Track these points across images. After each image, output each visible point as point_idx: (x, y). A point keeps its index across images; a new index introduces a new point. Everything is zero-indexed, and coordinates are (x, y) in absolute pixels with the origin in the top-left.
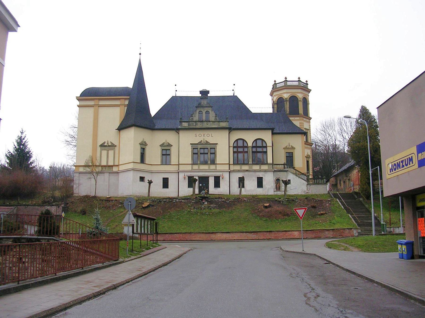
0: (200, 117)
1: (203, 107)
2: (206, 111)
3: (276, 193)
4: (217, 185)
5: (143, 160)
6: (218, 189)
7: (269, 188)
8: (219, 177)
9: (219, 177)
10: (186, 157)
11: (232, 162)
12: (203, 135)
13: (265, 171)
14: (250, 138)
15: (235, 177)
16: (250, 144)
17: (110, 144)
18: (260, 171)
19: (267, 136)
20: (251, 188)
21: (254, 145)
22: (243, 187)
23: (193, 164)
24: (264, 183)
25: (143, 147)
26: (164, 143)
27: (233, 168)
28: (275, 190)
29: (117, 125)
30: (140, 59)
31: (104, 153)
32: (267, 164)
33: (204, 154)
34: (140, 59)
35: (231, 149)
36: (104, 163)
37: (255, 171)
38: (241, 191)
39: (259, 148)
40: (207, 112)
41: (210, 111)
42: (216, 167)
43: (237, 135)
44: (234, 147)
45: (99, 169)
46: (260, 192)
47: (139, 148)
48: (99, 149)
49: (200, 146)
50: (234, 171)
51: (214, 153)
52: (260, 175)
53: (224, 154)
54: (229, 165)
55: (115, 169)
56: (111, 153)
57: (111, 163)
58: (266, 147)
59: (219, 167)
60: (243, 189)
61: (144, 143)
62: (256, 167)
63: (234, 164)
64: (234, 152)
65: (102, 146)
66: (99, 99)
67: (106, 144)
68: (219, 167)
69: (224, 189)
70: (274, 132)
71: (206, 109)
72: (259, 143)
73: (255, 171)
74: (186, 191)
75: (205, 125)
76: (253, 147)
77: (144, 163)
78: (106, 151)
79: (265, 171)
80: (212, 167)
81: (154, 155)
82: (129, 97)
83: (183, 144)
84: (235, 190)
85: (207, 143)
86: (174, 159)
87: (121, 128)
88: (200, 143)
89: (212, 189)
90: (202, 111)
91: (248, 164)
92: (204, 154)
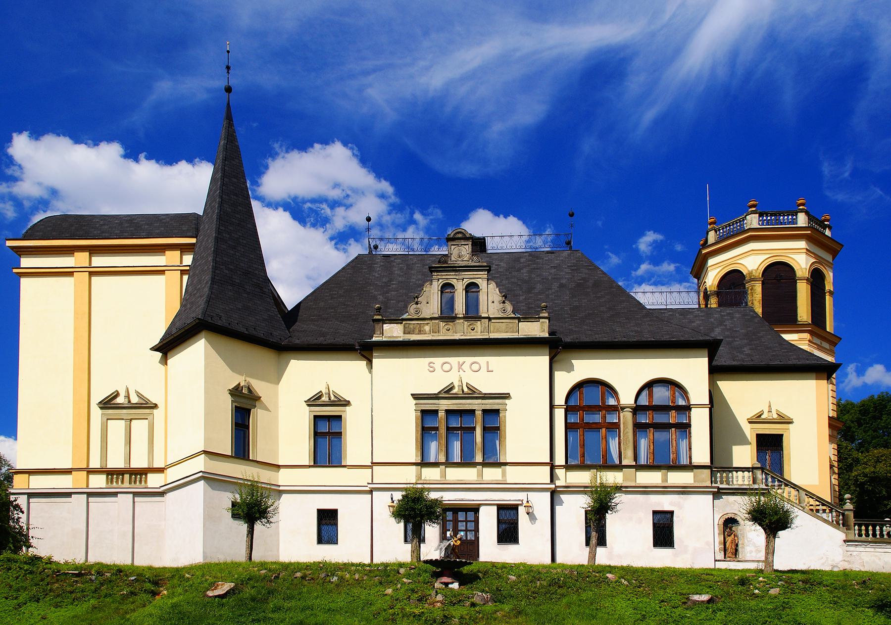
0: (448, 306)
1: (456, 269)
2: (466, 282)
3: (720, 565)
4: (508, 533)
5: (241, 448)
6: (511, 548)
7: (697, 546)
8: (514, 508)
9: (514, 508)
10: (400, 437)
11: (560, 459)
12: (455, 367)
13: (684, 490)
14: (627, 375)
15: (574, 509)
16: (627, 398)
17: (135, 399)
18: (665, 490)
19: (691, 372)
20: (629, 543)
21: (644, 401)
22: (602, 542)
23: (424, 463)
24: (679, 532)
25: (245, 404)
26: (319, 396)
27: (565, 478)
28: (720, 556)
29: (157, 334)
30: (228, 104)
31: (117, 428)
32: (690, 467)
33: (462, 427)
34: (228, 104)
35: (560, 414)
36: (116, 461)
37: (646, 490)
38: (593, 556)
39: (661, 413)
40: (471, 288)
41: (482, 284)
42: (504, 474)
43: (586, 368)
44: (569, 410)
45: (99, 482)
46: (662, 558)
47: (226, 405)
48: (97, 413)
49: (444, 405)
50: (570, 489)
51: (716, 561)
52: (665, 502)
53: (530, 429)
54: (553, 467)
55: (154, 481)
56: (140, 427)
57: (139, 462)
58: (688, 408)
59: (514, 475)
60: (600, 550)
61: (245, 391)
62: (653, 478)
63: (568, 467)
64: (568, 427)
65: (108, 404)
66: (94, 251)
67: (120, 400)
68: (514, 475)
69: (530, 549)
70: (724, 357)
71: (469, 277)
72: (661, 395)
73: (646, 490)
74: (392, 546)
75: (461, 331)
76: (637, 409)
77: (248, 459)
78: (122, 423)
79: (684, 490)
80: (491, 474)
81: (285, 432)
82: (193, 241)
83: (383, 396)
84: (573, 551)
85: (472, 394)
86: (355, 446)
87: (167, 347)
88: (447, 393)
89: (490, 550)
90: (454, 282)
91: (619, 467)
92: (462, 427)
